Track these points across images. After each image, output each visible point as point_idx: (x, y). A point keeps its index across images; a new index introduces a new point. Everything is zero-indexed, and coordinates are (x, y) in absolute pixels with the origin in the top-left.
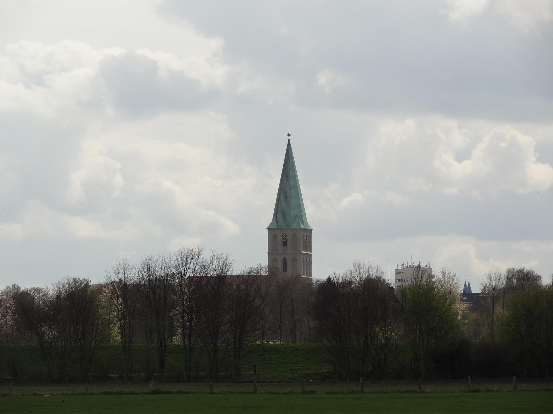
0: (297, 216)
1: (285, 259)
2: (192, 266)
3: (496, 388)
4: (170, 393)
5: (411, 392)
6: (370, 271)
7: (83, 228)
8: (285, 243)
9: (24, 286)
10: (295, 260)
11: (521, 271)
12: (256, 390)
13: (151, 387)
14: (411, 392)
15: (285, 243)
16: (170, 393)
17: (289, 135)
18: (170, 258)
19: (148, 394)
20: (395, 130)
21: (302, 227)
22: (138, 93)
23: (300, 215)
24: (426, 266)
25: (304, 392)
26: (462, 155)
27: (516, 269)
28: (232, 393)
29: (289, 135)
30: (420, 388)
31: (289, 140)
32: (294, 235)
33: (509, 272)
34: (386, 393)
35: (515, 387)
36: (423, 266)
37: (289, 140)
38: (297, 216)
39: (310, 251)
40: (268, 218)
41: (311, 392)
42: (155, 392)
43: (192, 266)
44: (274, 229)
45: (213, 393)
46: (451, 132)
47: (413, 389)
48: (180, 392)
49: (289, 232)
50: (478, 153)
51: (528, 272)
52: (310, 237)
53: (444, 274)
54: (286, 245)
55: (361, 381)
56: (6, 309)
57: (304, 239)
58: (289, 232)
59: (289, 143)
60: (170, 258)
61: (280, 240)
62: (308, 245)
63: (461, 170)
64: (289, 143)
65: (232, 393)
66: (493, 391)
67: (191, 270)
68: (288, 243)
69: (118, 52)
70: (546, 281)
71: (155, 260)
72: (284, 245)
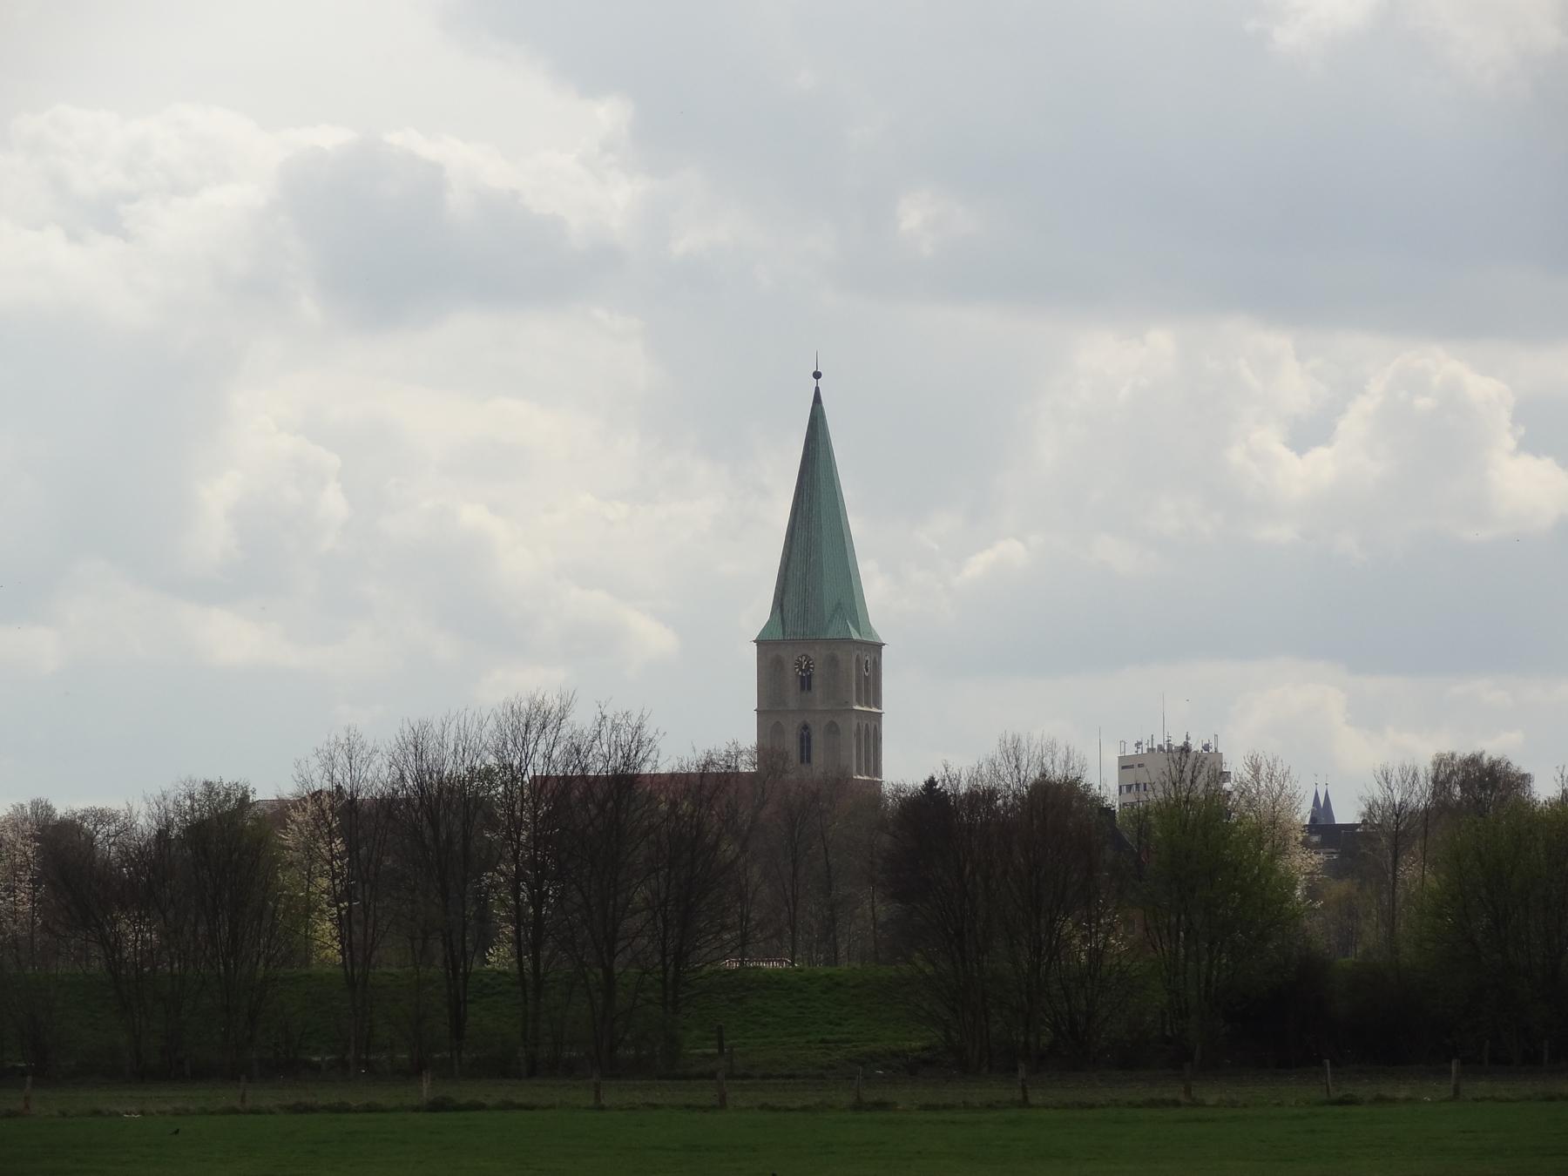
0: (839, 606)
1: (806, 727)
2: (542, 747)
3: (1403, 1092)
4: (481, 1107)
5: (1164, 1103)
6: (1047, 761)
7: (233, 638)
8: (806, 683)
9: (64, 805)
10: (833, 729)
11: (1474, 761)
12: (723, 1098)
13: (426, 1089)
14: (1164, 1103)
15: (806, 683)
16: (481, 1107)
17: (817, 375)
18: (481, 726)
19: (416, 1109)
20: (1117, 362)
21: (855, 636)
22: (389, 256)
23: (849, 603)
24: (1206, 748)
25: (858, 1106)
26: (1308, 433)
27: (1459, 756)
28: (655, 1106)
29: (817, 375)
30: (1188, 1091)
31: (817, 389)
32: (833, 661)
33: (1440, 763)
34: (1092, 1106)
35: (1457, 1091)
36: (1196, 746)
37: (817, 389)
38: (839, 606)
39: (878, 704)
40: (757, 610)
41: (881, 1105)
42: (437, 1106)
43: (542, 747)
44: (777, 643)
45: (602, 1108)
46: (1278, 366)
47: (1168, 1096)
48: (507, 1106)
49: (816, 650)
50: (1353, 424)
51: (1493, 765)
52: (877, 665)
53: (1257, 770)
54: (809, 688)
55: (1022, 1074)
56: (14, 868)
57: (858, 669)
58: (816, 650)
59: (817, 399)
60: (481, 726)
61: (791, 674)
62: (871, 688)
63: (1305, 474)
64: (817, 399)
65: (655, 1106)
66: (1393, 1101)
67: (538, 760)
68: (816, 681)
69: (330, 137)
70: (1544, 790)
71: (437, 729)
72: (803, 688)
